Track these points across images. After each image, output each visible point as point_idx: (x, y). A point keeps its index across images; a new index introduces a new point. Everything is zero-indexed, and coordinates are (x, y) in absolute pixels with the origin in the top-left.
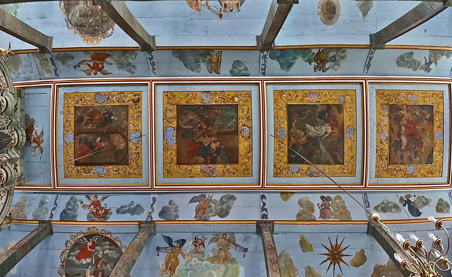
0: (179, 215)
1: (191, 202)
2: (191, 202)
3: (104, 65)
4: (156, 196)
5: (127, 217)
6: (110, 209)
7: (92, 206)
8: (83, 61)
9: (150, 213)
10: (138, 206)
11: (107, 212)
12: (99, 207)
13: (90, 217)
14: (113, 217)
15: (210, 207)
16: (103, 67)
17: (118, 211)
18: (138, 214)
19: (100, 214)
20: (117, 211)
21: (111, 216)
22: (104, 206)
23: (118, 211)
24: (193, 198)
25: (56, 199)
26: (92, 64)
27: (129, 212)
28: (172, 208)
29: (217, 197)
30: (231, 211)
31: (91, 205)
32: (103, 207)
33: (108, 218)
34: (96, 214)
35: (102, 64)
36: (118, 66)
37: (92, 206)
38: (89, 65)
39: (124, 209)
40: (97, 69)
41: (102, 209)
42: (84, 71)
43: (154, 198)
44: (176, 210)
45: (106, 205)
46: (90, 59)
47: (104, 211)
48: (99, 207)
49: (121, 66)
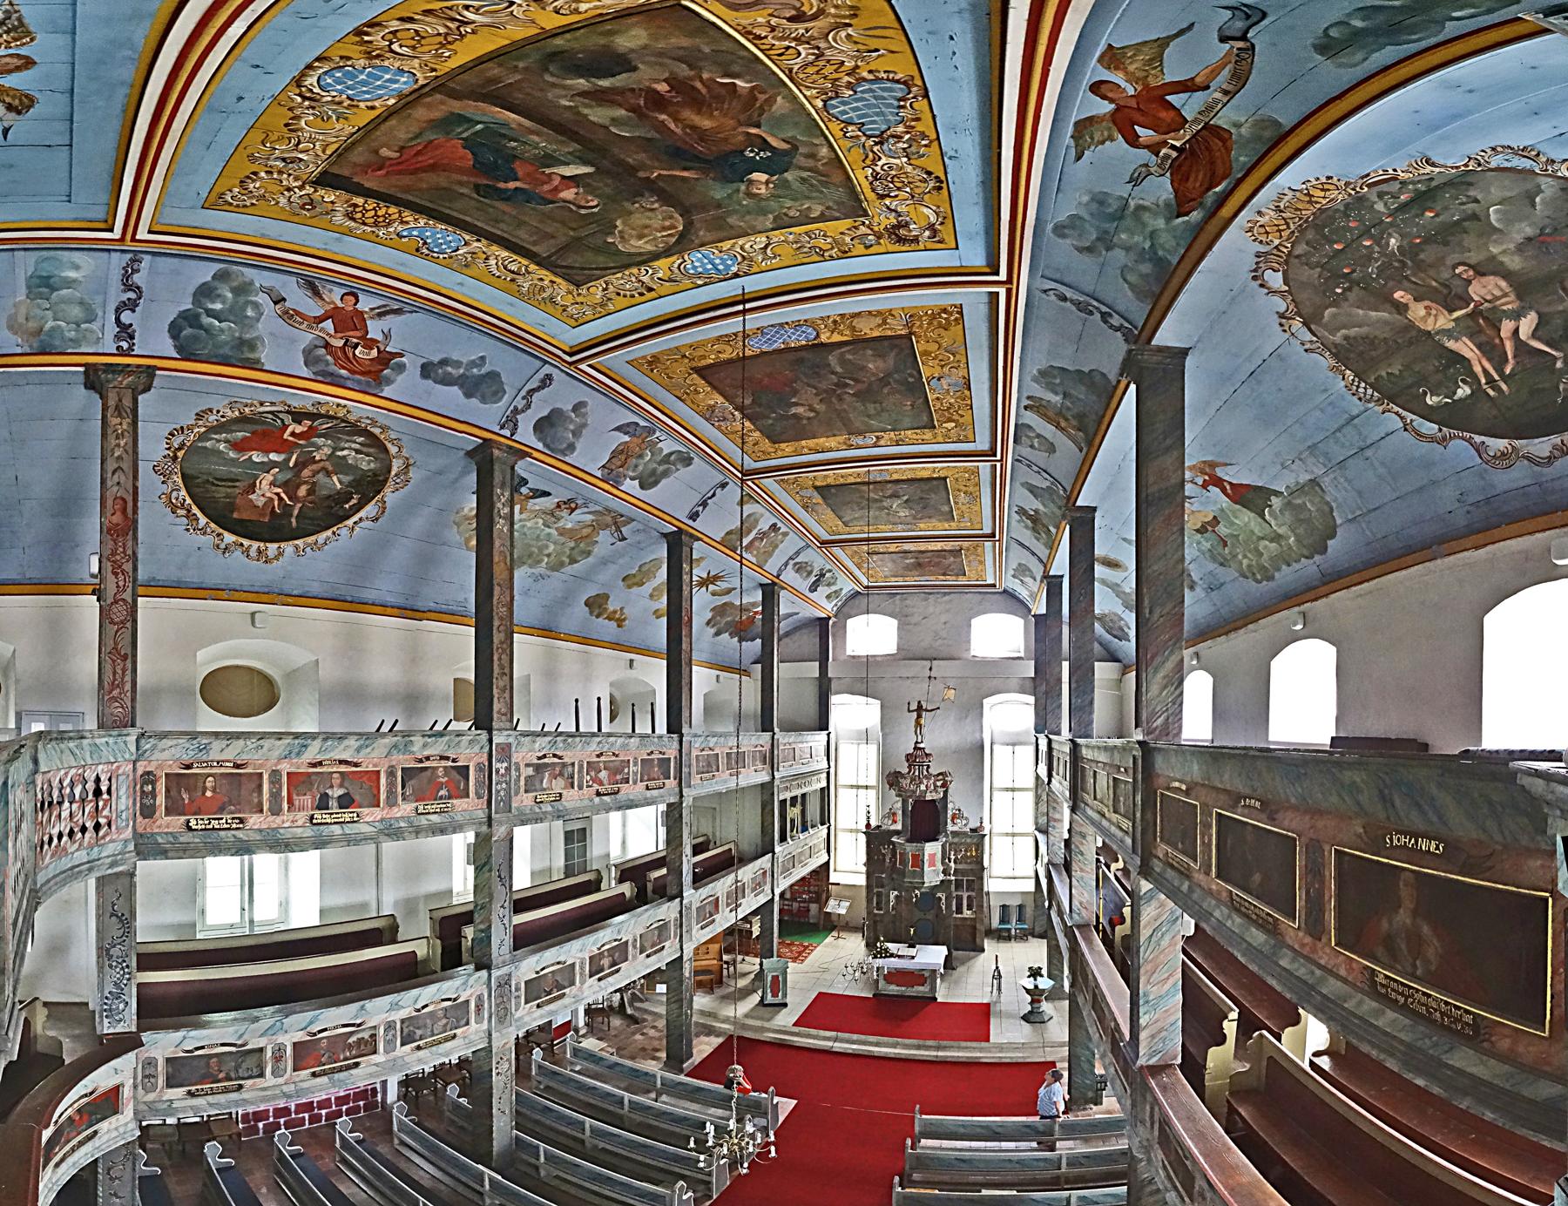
0: (579, 446)
1: (618, 429)
2: (618, 429)
3: (1144, 155)
4: (555, 372)
5: (450, 398)
6: (402, 356)
7: (328, 325)
8: (1240, 79)
9: (516, 411)
10: (494, 376)
11: (385, 359)
12: (358, 334)
13: (318, 360)
14: (404, 385)
15: (641, 456)
16: (1133, 140)
17: (427, 370)
18: (484, 400)
19: (354, 355)
20: (423, 366)
21: (400, 378)
22: (380, 337)
23: (427, 370)
24: (628, 425)
25: (845, 830)
26: (1189, 105)
27: (461, 387)
28: (572, 421)
29: (667, 446)
30: (664, 482)
31: (321, 319)
32: (374, 341)
33: (389, 382)
34: (344, 355)
35: (1154, 149)
36: (1114, 206)
37: (328, 325)
38: (1187, 86)
39: (449, 369)
40: (1140, 113)
41: (370, 344)
42: (1163, 43)
43: (549, 377)
44: (577, 433)
45: (387, 336)
46: (1221, 121)
47: (374, 353)
48: (358, 334)
49: (1109, 218)
